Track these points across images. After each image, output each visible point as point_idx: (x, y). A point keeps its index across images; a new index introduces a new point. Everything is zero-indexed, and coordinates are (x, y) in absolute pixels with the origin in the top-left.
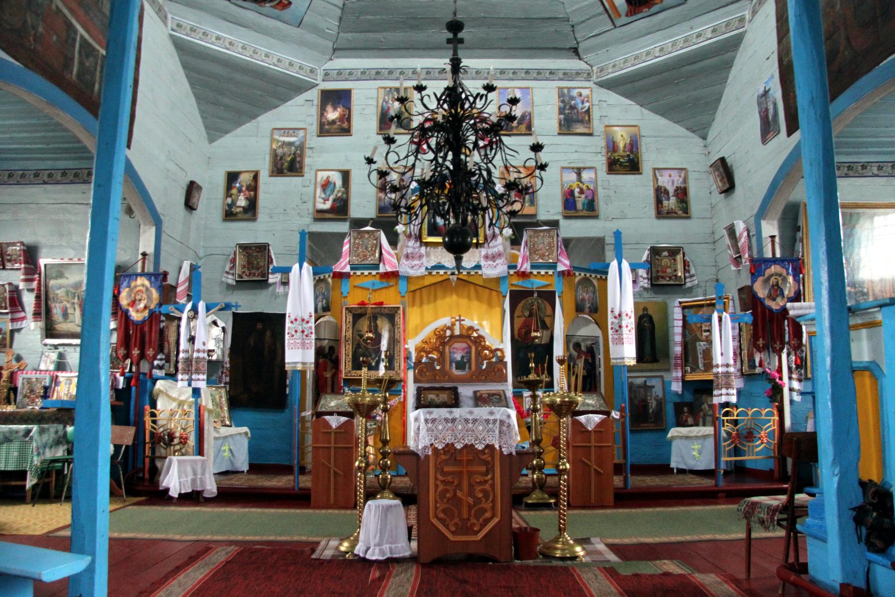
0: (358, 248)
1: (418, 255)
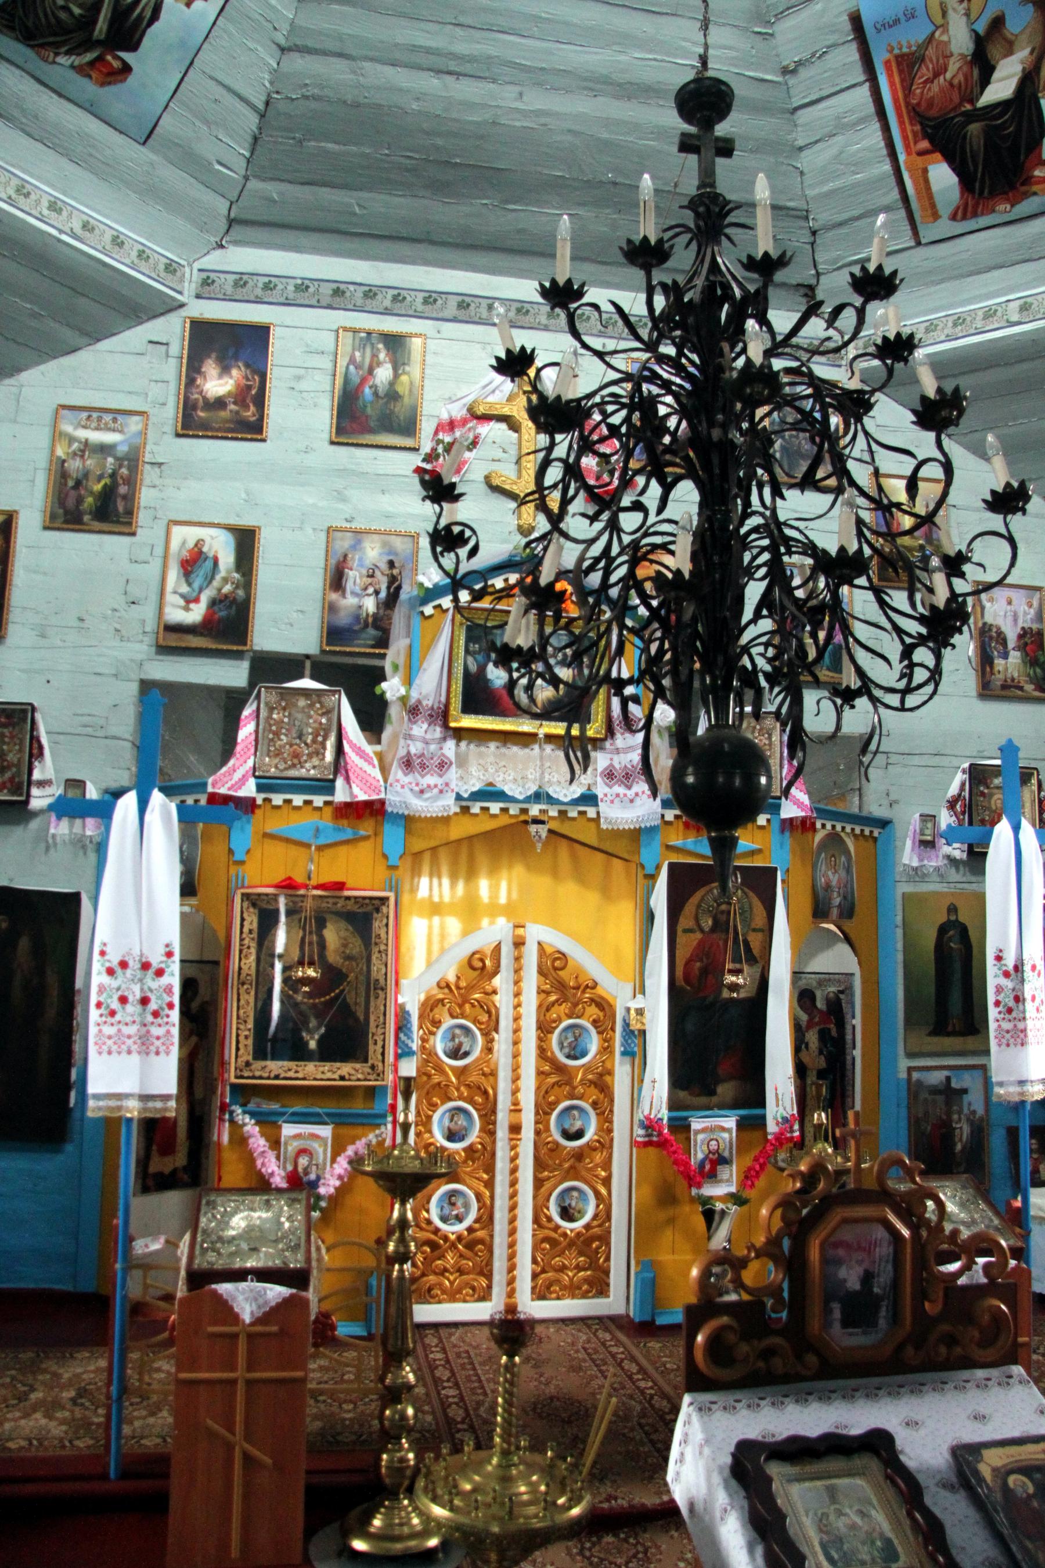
0: (277, 734)
1: (436, 761)
